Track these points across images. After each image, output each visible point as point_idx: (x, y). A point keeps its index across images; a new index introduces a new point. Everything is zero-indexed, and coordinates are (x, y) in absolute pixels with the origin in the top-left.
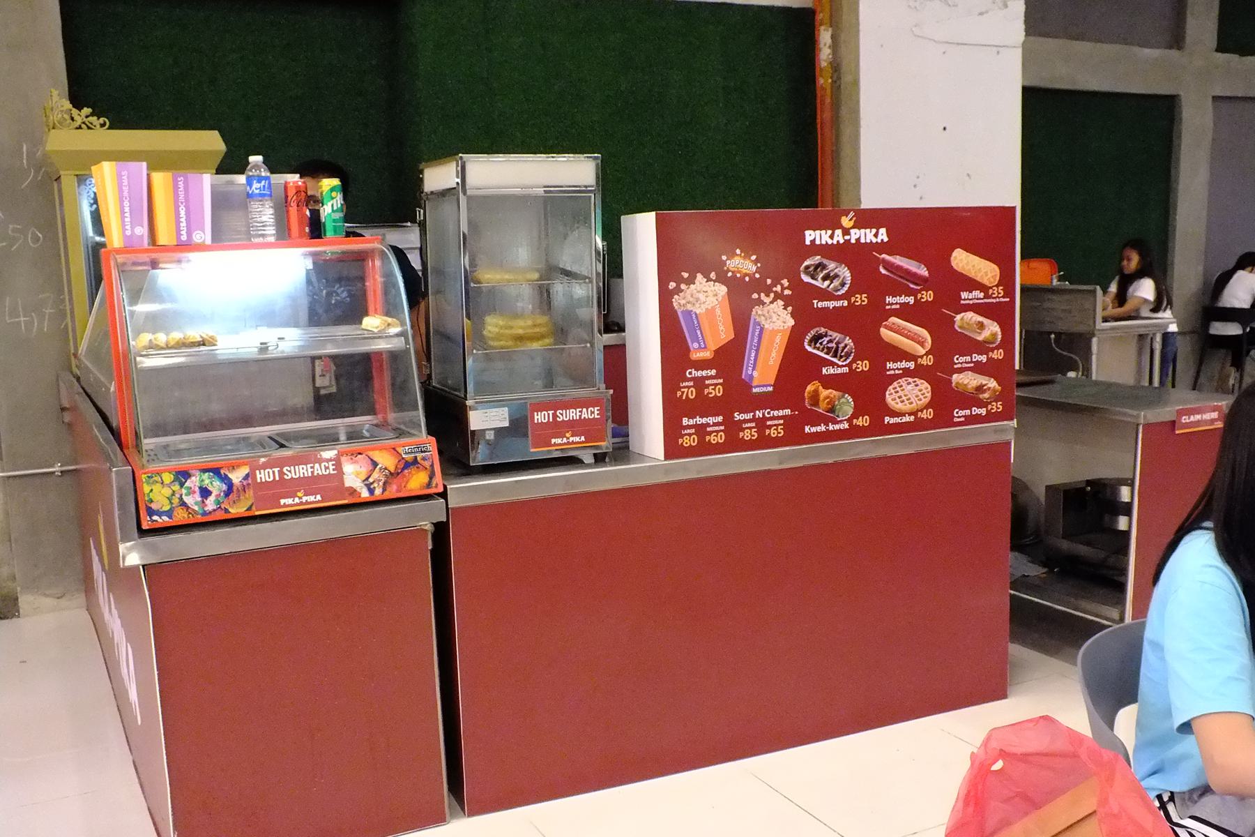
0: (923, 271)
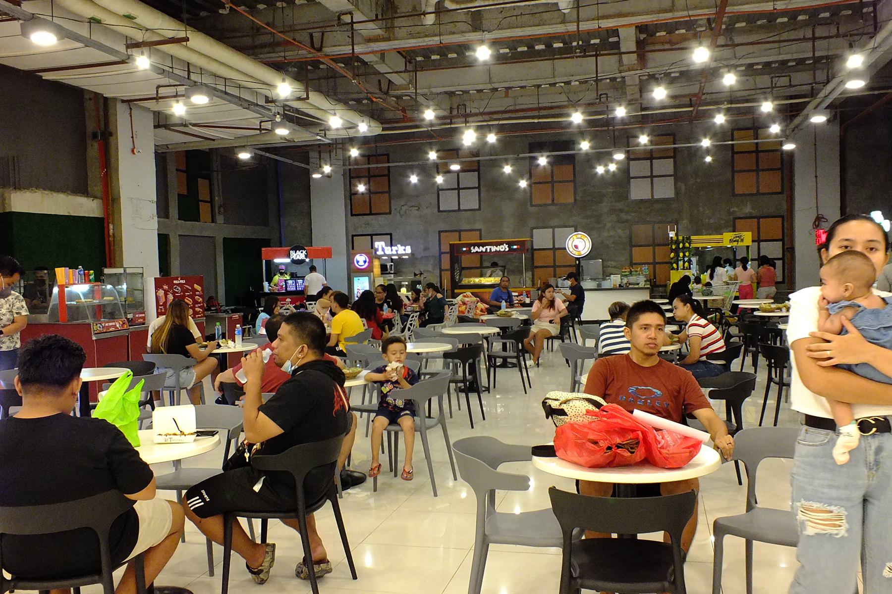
0: (190, 288)
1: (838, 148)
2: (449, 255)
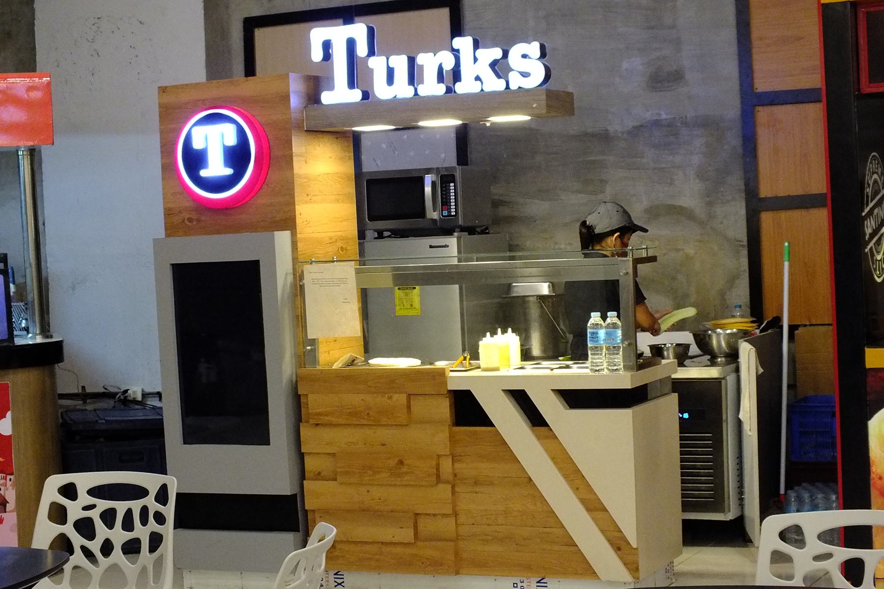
1: (302, 439)
2: (815, 112)
